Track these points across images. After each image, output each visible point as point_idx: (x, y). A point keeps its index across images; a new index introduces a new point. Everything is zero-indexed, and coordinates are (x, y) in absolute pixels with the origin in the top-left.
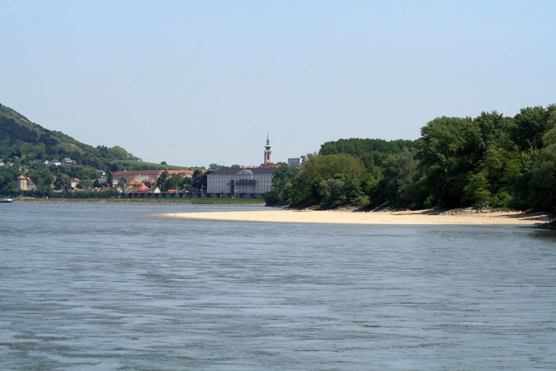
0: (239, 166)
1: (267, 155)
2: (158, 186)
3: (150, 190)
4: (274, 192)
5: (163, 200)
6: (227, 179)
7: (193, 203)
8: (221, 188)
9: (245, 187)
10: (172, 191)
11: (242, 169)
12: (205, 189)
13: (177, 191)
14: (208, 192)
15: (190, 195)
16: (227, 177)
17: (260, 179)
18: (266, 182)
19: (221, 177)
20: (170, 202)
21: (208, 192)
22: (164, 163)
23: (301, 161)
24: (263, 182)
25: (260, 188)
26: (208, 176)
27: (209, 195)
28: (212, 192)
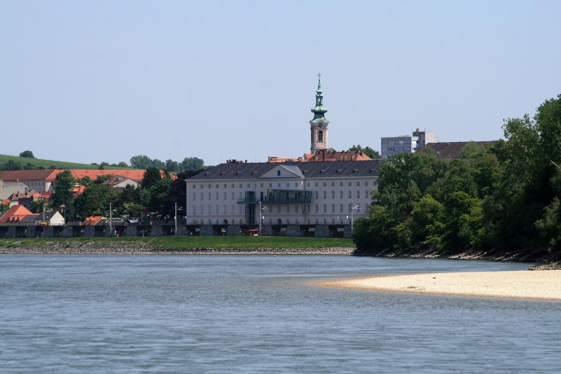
0: (201, 162)
1: (318, 130)
2: (55, 207)
3: (40, 218)
4: (383, 220)
5: (76, 242)
6: (239, 189)
7: (156, 250)
8: (214, 213)
9: (284, 209)
10: (95, 220)
11: (277, 164)
12: (183, 213)
13: (109, 220)
14: (189, 221)
15: (143, 230)
16: (237, 184)
17: (321, 189)
18: (337, 195)
19: (221, 185)
20: (96, 247)
21: (189, 221)
22: (27, 154)
23: (414, 144)
24: (329, 195)
25: (321, 211)
26: (190, 184)
27: (193, 230)
28: (199, 222)
